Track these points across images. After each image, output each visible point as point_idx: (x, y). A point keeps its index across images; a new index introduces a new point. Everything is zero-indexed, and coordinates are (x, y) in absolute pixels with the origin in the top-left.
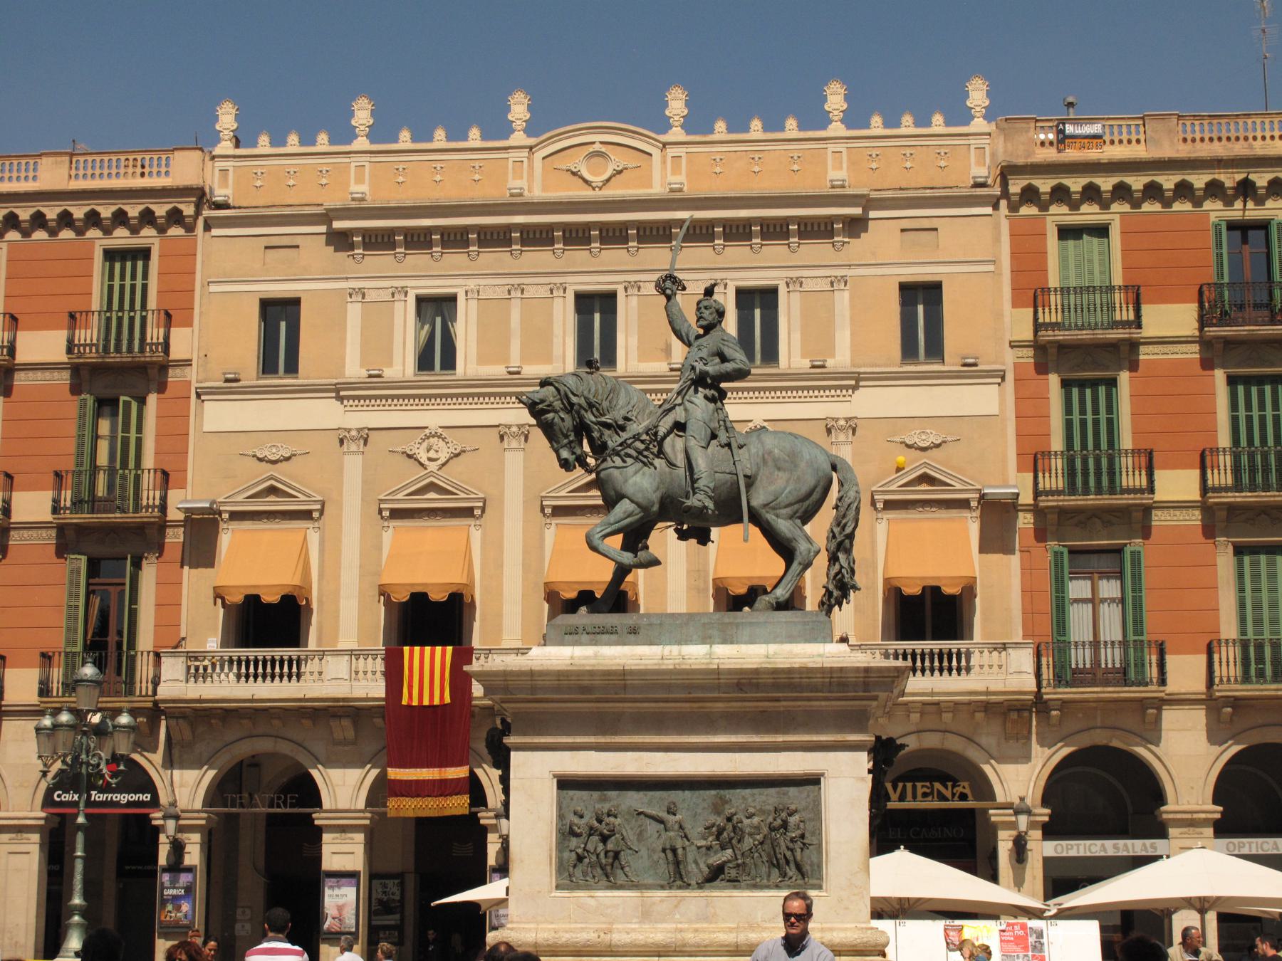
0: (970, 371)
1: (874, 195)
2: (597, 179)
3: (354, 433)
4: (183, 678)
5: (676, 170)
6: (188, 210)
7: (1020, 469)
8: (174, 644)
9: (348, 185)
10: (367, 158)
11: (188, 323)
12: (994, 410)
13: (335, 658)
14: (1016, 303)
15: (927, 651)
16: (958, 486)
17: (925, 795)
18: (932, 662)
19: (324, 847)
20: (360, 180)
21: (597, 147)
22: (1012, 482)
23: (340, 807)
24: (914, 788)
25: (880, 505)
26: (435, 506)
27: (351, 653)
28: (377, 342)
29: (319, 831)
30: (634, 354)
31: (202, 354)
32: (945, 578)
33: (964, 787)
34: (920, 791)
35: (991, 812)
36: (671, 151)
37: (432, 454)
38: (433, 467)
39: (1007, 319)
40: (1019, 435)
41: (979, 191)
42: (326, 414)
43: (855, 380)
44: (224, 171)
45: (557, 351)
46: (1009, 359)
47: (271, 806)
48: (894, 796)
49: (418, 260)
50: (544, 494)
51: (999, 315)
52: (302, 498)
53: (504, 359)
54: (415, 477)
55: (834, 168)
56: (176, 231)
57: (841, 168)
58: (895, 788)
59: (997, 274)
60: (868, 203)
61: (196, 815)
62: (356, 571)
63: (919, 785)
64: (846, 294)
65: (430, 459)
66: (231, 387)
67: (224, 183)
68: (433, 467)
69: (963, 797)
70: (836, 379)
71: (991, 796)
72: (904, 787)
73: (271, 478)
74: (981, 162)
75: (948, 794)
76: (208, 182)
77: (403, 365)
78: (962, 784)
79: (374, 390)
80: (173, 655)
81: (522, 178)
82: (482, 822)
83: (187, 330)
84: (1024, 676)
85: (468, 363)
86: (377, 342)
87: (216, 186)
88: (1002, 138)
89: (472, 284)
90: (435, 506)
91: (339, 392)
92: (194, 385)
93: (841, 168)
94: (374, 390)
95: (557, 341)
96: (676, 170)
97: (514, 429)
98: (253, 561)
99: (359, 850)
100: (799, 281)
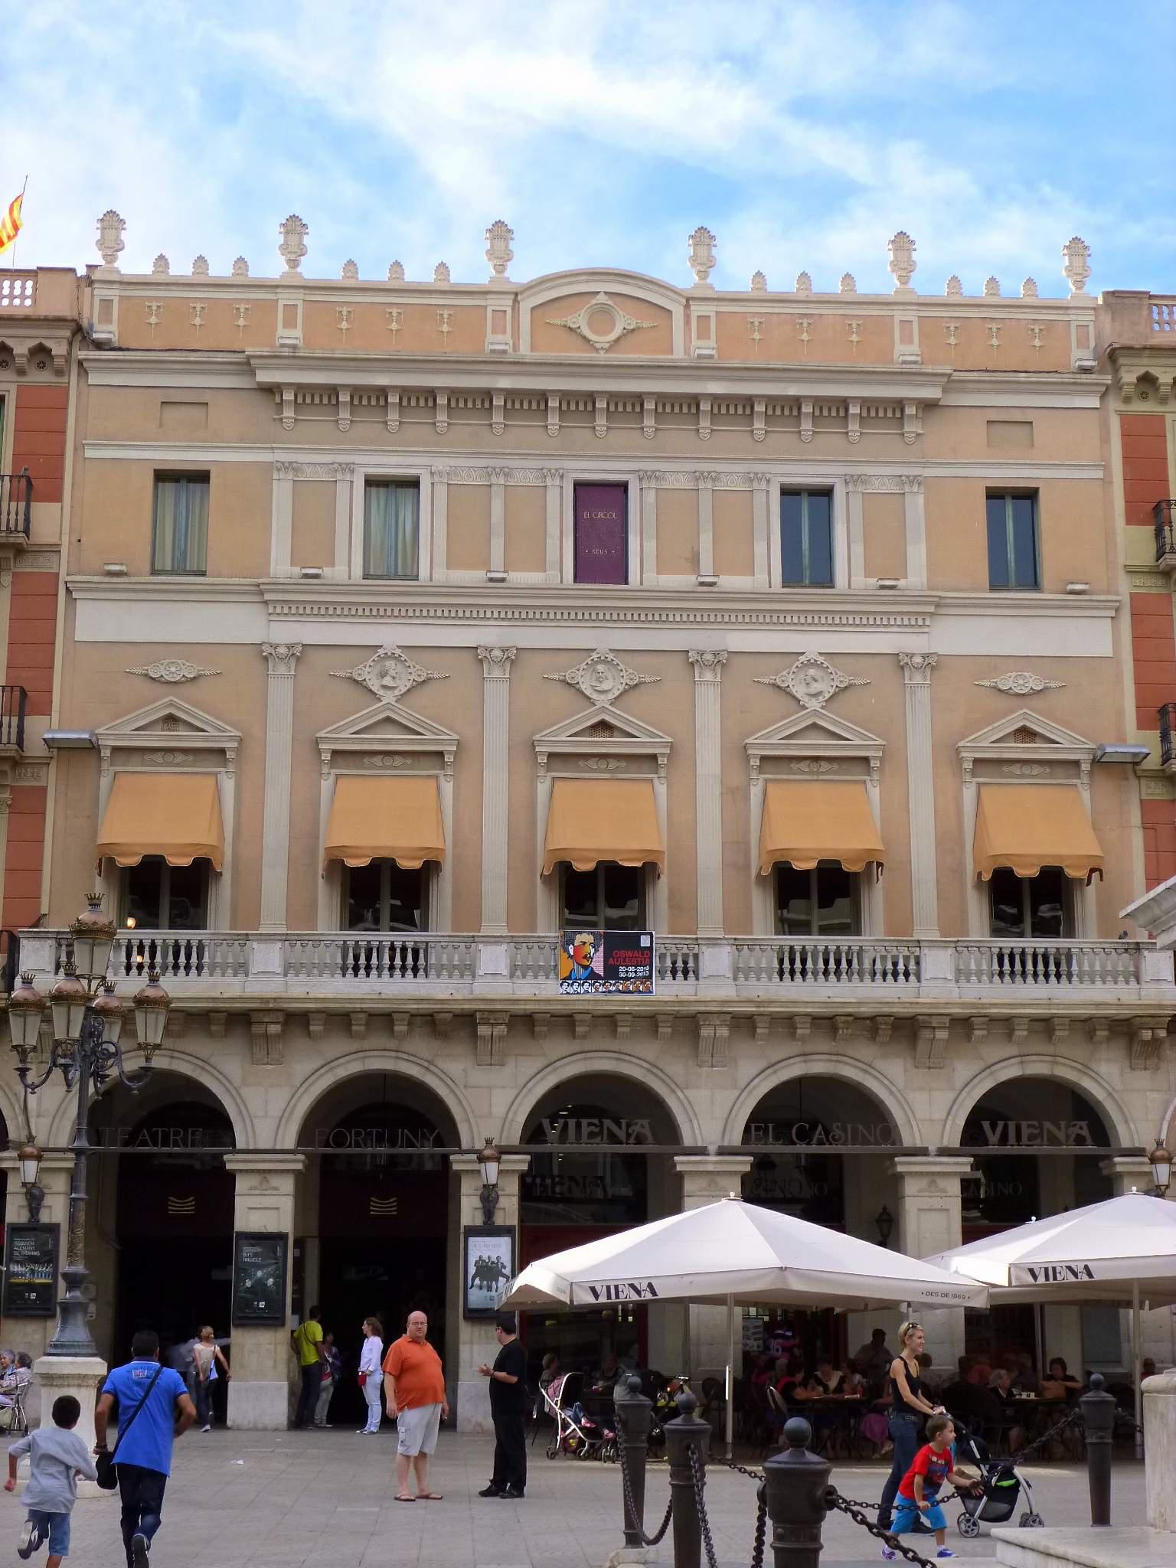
0: (1078, 599)
1: (957, 376)
2: (603, 340)
3: (282, 650)
4: (51, 967)
5: (703, 334)
6: (58, 349)
7: (1142, 725)
8: (33, 920)
9: (275, 329)
10: (300, 295)
11: (56, 496)
12: (1107, 651)
13: (263, 946)
14: (1131, 519)
15: (375, 944)
16: (213, 732)
17: (591, 1135)
18: (404, 959)
19: (237, 1199)
20: (290, 323)
21: (602, 299)
22: (1130, 741)
23: (261, 1146)
24: (578, 1126)
25: (326, 757)
26: (605, 752)
27: (285, 938)
28: (313, 534)
29: (231, 1177)
30: (651, 562)
31: (74, 541)
32: (366, 848)
33: (642, 1126)
34: (585, 1130)
35: (1117, 1159)
36: (697, 310)
37: (387, 681)
38: (389, 698)
39: (1120, 539)
40: (1138, 683)
41: (1084, 378)
42: (238, 624)
43: (933, 607)
44: (107, 303)
45: (552, 555)
46: (1125, 587)
47: (327, 1145)
48: (993, 1138)
49: (782, 439)
50: (537, 737)
51: (1109, 535)
52: (213, 732)
53: (485, 564)
54: (371, 712)
55: (902, 342)
56: (44, 377)
57: (911, 342)
58: (994, 1129)
59: (1106, 482)
60: (950, 384)
61: (61, 1155)
62: (285, 830)
63: (584, 1122)
64: (921, 499)
65: (384, 687)
66: (114, 581)
67: (106, 317)
68: (389, 698)
69: (639, 1141)
70: (447, 595)
71: (456, 1141)
72: (1006, 1127)
73: (171, 704)
74: (1082, 343)
75: (1061, 1136)
76: (86, 314)
77: (347, 565)
78: (640, 1122)
79: (308, 596)
80: (37, 936)
81: (504, 332)
82: (679, 1168)
83: (53, 507)
84: (1164, 985)
85: (433, 564)
86: (313, 534)
87: (95, 320)
88: (1109, 316)
89: (440, 464)
90: (605, 752)
91: (261, 594)
92: (63, 577)
93: (911, 342)
94: (500, 601)
95: (552, 544)
96: (703, 334)
97: (497, 653)
98: (153, 818)
99: (287, 1204)
100: (653, 475)
